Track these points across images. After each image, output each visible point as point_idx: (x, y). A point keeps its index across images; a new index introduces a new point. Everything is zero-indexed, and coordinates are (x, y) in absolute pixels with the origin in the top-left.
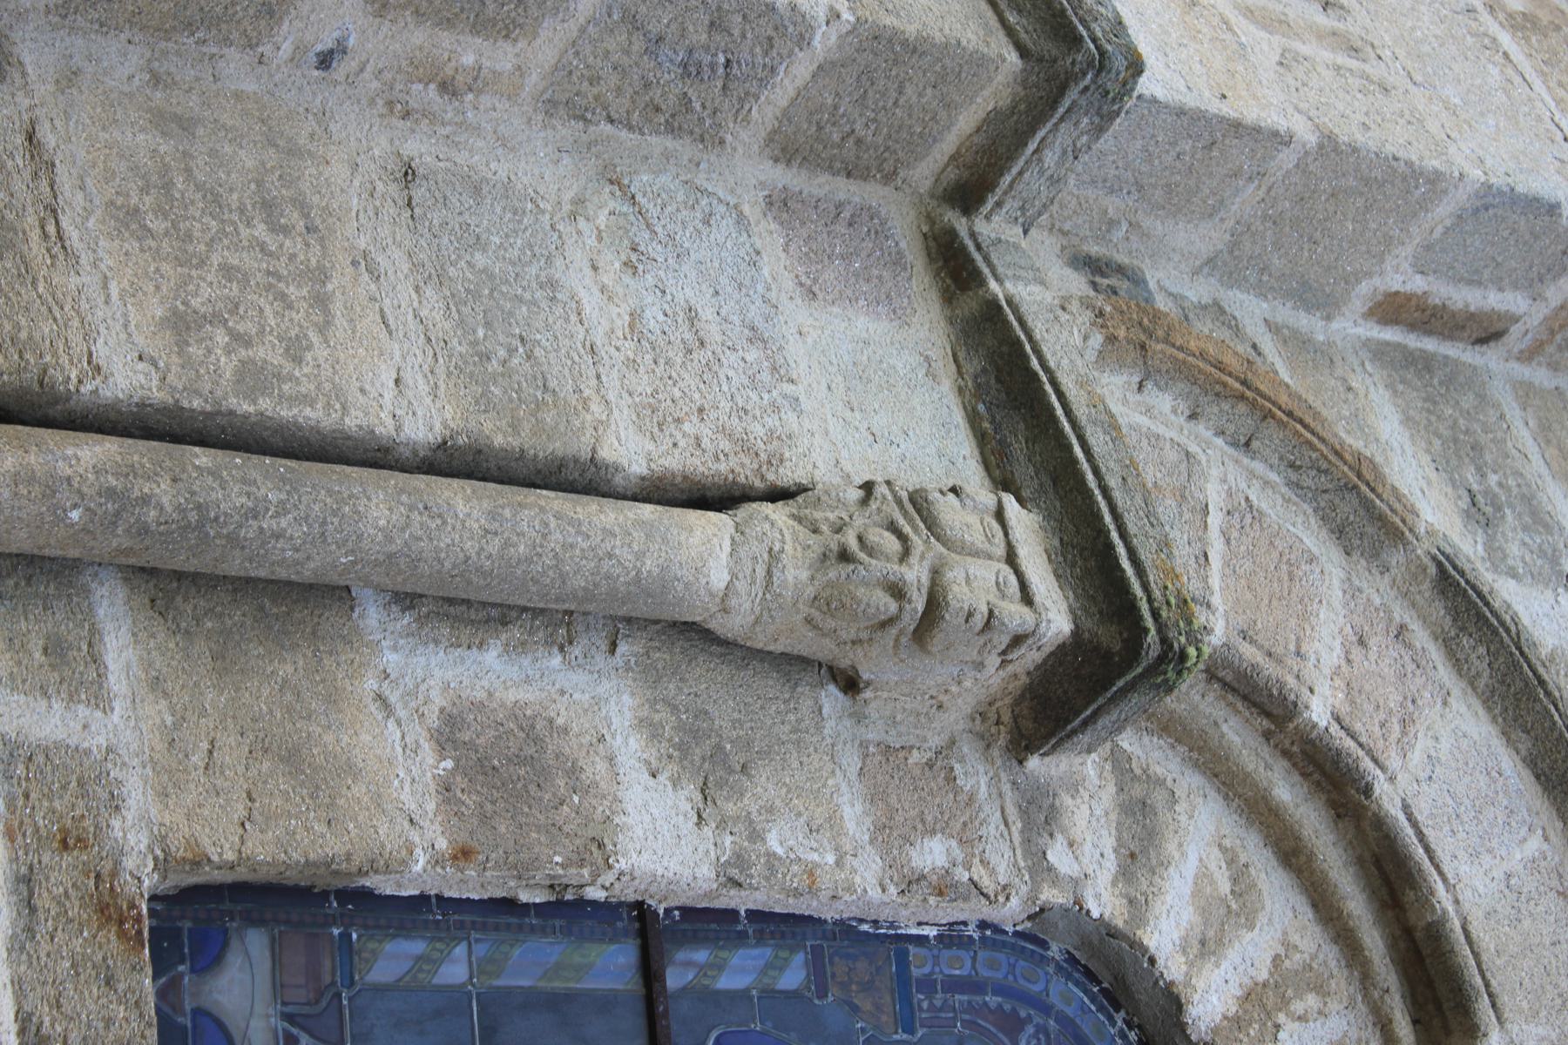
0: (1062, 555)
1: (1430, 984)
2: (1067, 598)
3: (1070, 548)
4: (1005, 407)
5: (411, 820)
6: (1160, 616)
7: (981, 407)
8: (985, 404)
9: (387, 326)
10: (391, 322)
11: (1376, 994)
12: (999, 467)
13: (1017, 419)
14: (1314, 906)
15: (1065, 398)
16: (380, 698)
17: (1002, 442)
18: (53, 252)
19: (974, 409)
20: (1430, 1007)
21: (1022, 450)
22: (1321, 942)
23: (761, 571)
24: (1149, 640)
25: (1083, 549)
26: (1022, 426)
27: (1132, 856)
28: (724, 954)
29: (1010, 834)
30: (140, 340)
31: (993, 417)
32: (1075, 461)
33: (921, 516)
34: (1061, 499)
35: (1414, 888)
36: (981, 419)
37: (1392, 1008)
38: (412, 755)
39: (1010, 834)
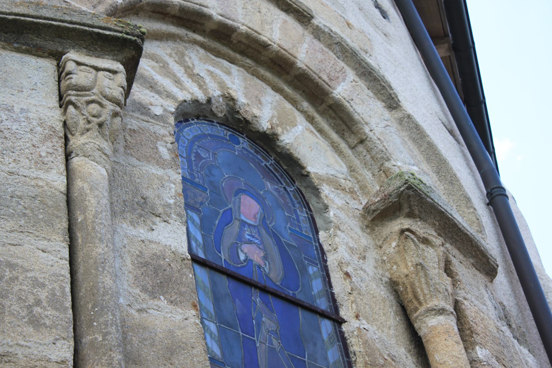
0: (90, 51)
1: (189, 20)
2: (108, 59)
3: (89, 47)
4: (20, 37)
5: (186, 319)
6: (128, 33)
7: (16, 45)
8: (14, 43)
9: (16, 245)
10: (15, 243)
11: (186, 38)
12: (44, 53)
13: (26, 36)
14: (157, 39)
15: (26, 15)
16: (140, 311)
17: (35, 46)
18: (7, 361)
19: (15, 48)
20: (194, 25)
21: (41, 41)
22: (167, 45)
23: (104, 157)
24: (138, 41)
25: (92, 43)
26: (30, 36)
27: (151, 87)
28: (192, 237)
29: (152, 123)
30: (47, 341)
31: (21, 43)
32: (59, 27)
33: (80, 91)
34: (68, 39)
35: (169, 6)
36: (21, 48)
37: (192, 37)
38: (161, 309)
39: (152, 123)
